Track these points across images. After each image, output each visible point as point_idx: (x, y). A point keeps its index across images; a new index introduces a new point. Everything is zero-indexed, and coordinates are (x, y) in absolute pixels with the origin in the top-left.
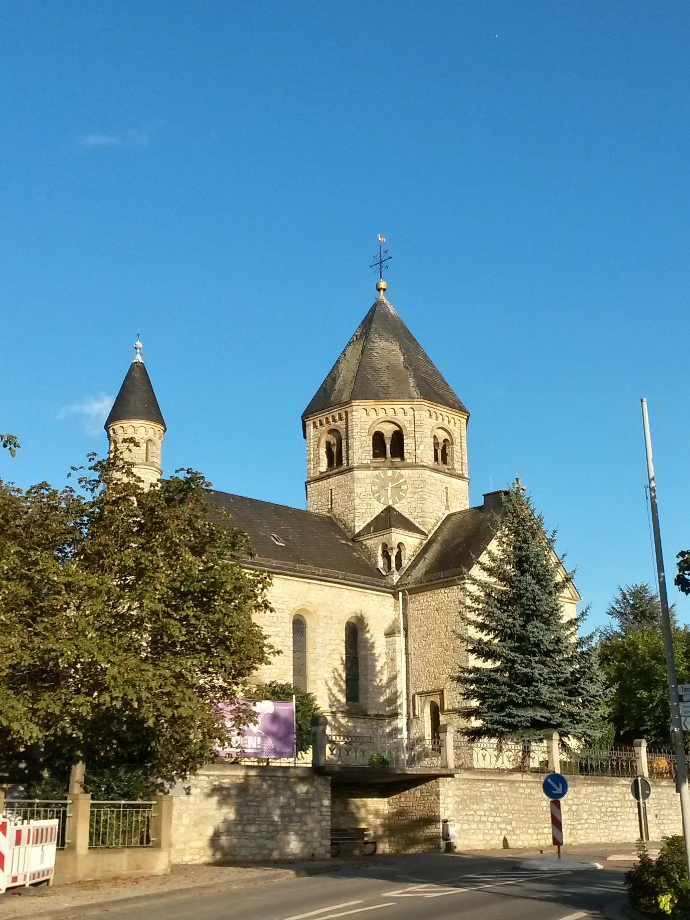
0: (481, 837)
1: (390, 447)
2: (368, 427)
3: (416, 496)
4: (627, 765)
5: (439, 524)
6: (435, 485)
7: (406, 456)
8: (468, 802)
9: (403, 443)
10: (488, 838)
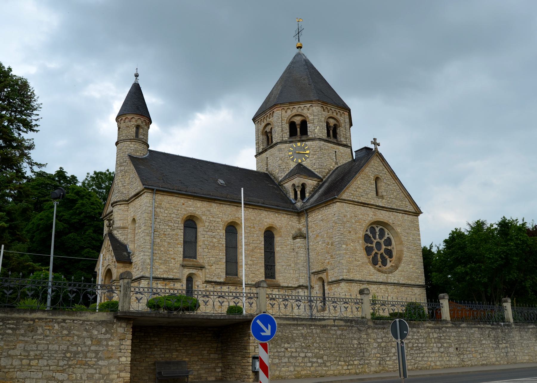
1: (298, 130)
3: (315, 157)
4: (477, 314)
5: (331, 172)
6: (328, 149)
7: (309, 133)
8: (279, 342)
9: (307, 126)
10: (299, 369)
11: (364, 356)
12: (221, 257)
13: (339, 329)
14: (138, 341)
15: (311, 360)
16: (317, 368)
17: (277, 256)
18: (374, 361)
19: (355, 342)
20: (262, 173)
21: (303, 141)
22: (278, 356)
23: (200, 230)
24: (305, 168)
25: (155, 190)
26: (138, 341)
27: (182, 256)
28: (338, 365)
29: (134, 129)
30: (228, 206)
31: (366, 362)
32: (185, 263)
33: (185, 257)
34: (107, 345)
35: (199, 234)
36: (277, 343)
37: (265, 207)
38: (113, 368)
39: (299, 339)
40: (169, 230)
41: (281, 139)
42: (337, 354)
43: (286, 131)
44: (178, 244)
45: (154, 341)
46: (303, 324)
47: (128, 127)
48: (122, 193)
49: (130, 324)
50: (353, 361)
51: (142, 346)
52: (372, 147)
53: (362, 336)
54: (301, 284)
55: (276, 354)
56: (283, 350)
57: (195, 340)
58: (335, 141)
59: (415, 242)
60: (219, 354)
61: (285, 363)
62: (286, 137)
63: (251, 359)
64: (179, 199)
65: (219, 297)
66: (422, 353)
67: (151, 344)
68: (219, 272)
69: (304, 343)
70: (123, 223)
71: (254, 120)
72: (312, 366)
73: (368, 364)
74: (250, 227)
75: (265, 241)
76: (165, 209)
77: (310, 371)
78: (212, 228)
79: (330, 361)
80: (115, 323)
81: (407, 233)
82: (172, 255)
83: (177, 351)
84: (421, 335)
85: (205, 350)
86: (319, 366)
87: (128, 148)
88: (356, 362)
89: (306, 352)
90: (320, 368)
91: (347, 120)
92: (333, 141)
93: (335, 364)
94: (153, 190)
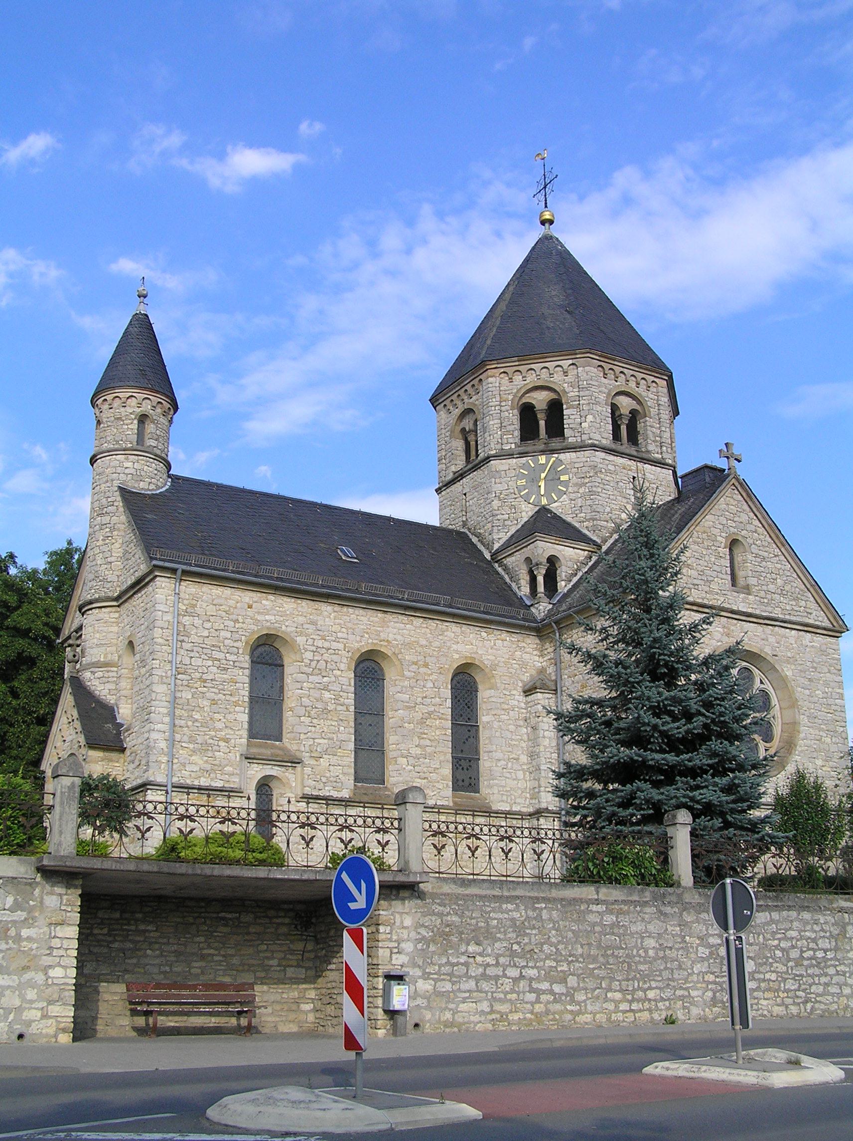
0: (485, 1006)
1: (542, 424)
2: (510, 397)
8: (454, 939)
10: (504, 1008)
11: (673, 980)
12: (342, 737)
13: (611, 912)
14: (105, 931)
15: (535, 985)
16: (550, 1007)
17: (483, 735)
18: (700, 993)
19: (651, 943)
20: (451, 531)
21: (553, 451)
22: (451, 975)
23: (291, 671)
24: (556, 517)
25: (179, 572)
26: (105, 931)
27: (245, 734)
28: (606, 1000)
29: (135, 425)
30: (361, 611)
31: (679, 993)
32: (254, 750)
33: (252, 735)
34: (18, 938)
35: (288, 680)
36: (449, 941)
37: (454, 615)
38: (31, 994)
39: (505, 933)
40: (214, 670)
41: (499, 446)
42: (602, 973)
43: (511, 428)
44: (236, 704)
45: (145, 931)
46: (518, 897)
47: (120, 419)
48: (105, 580)
49: (76, 887)
50: (645, 991)
51: (116, 945)
52: (722, 464)
53: (670, 928)
54: (544, 805)
55: (447, 969)
56: (463, 959)
57: (248, 933)
58: (632, 451)
59: (831, 701)
60: (307, 969)
61: (469, 991)
62: (512, 440)
63: (381, 979)
64: (239, 593)
65: (303, 826)
66: (826, 975)
67: (138, 938)
68: (337, 773)
69: (518, 943)
70: (106, 655)
71: (435, 401)
72: (538, 1001)
73: (681, 998)
74: (415, 663)
75: (454, 697)
76: (205, 618)
77: (532, 1013)
78: (322, 664)
79: (586, 989)
80: (38, 883)
81: (810, 680)
82: (221, 730)
83: (203, 957)
84: (822, 930)
85: (273, 958)
86: (555, 1001)
87: (119, 470)
88: (651, 994)
89: (523, 967)
90: (558, 1007)
91: (665, 400)
92: (627, 451)
93: (598, 998)
94: (174, 571)
